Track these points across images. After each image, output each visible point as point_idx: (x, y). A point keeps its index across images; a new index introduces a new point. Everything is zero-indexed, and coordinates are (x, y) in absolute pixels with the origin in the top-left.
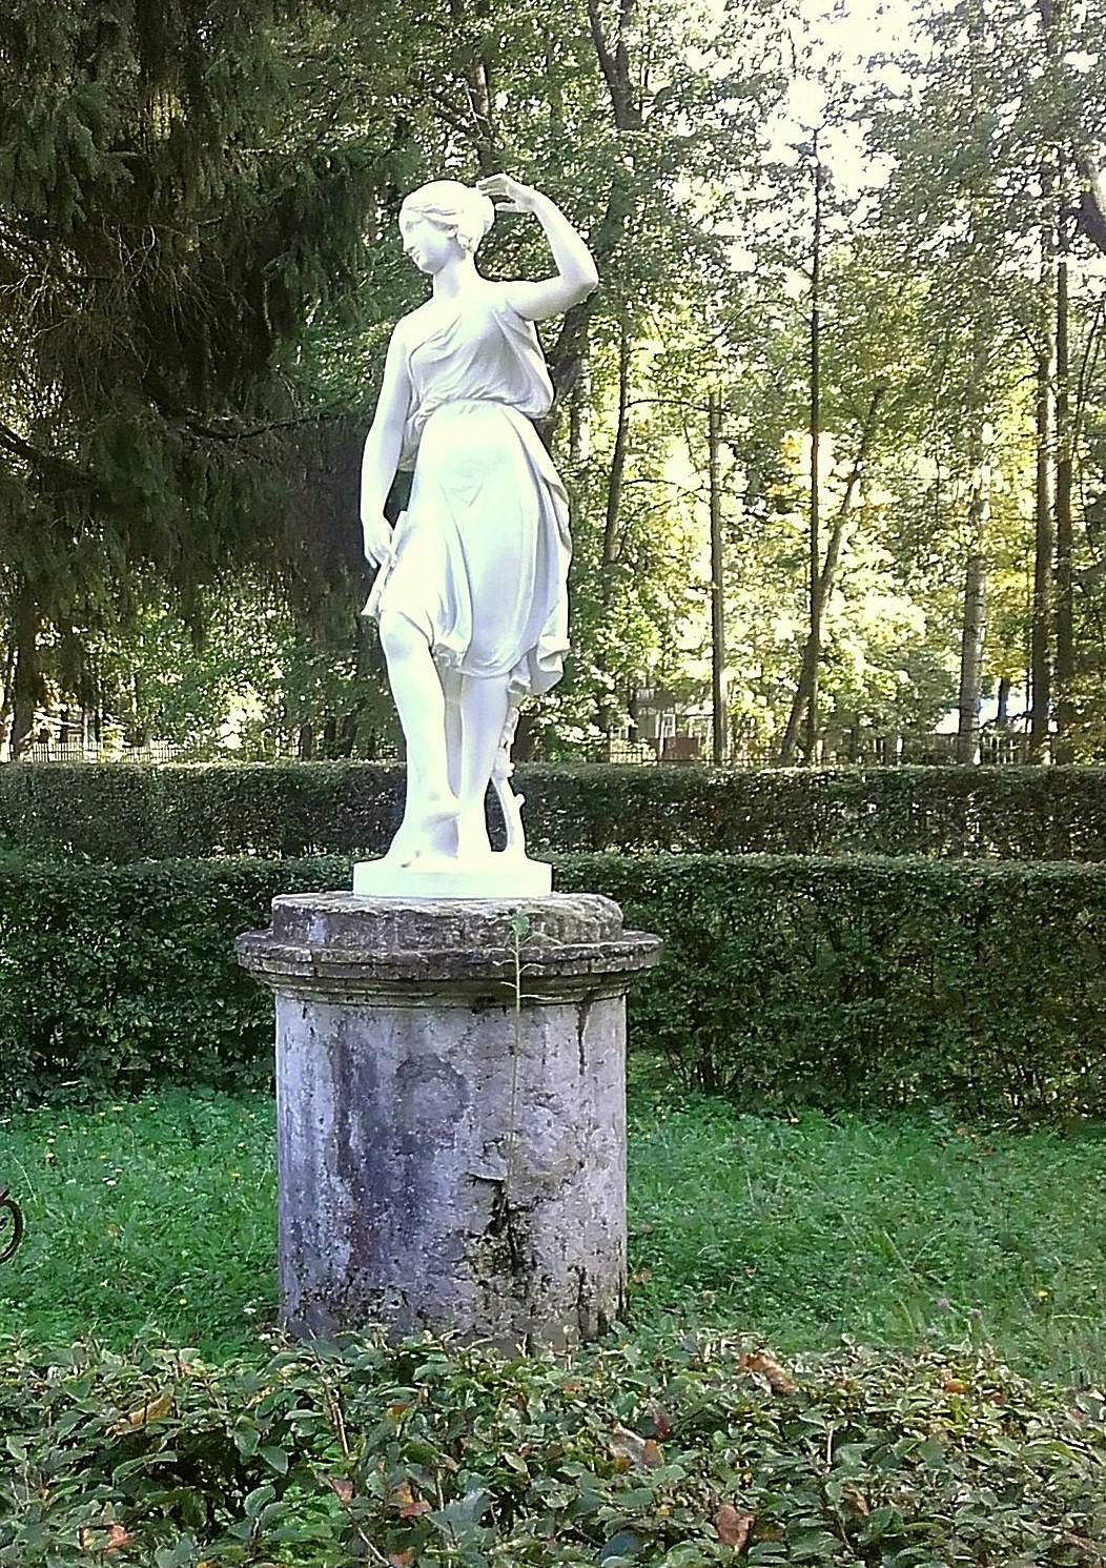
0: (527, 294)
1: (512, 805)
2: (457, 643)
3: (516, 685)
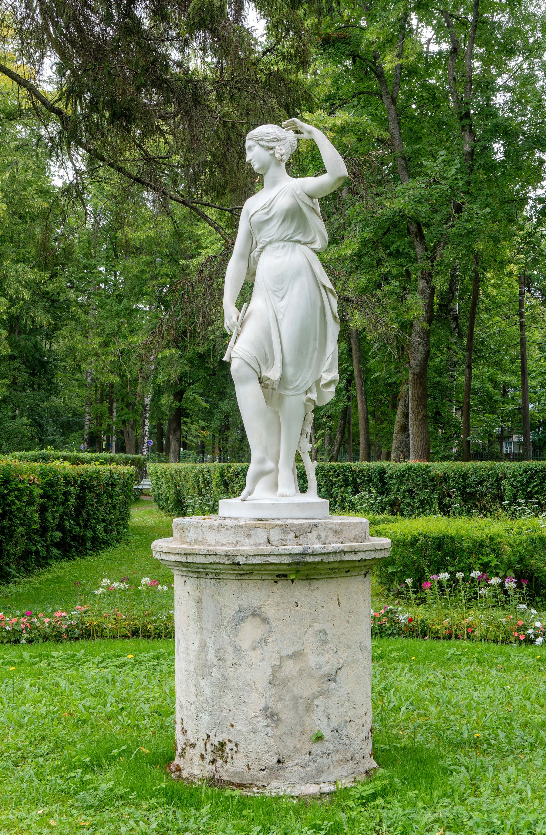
0: (310, 182)
1: (310, 467)
2: (273, 374)
3: (309, 400)
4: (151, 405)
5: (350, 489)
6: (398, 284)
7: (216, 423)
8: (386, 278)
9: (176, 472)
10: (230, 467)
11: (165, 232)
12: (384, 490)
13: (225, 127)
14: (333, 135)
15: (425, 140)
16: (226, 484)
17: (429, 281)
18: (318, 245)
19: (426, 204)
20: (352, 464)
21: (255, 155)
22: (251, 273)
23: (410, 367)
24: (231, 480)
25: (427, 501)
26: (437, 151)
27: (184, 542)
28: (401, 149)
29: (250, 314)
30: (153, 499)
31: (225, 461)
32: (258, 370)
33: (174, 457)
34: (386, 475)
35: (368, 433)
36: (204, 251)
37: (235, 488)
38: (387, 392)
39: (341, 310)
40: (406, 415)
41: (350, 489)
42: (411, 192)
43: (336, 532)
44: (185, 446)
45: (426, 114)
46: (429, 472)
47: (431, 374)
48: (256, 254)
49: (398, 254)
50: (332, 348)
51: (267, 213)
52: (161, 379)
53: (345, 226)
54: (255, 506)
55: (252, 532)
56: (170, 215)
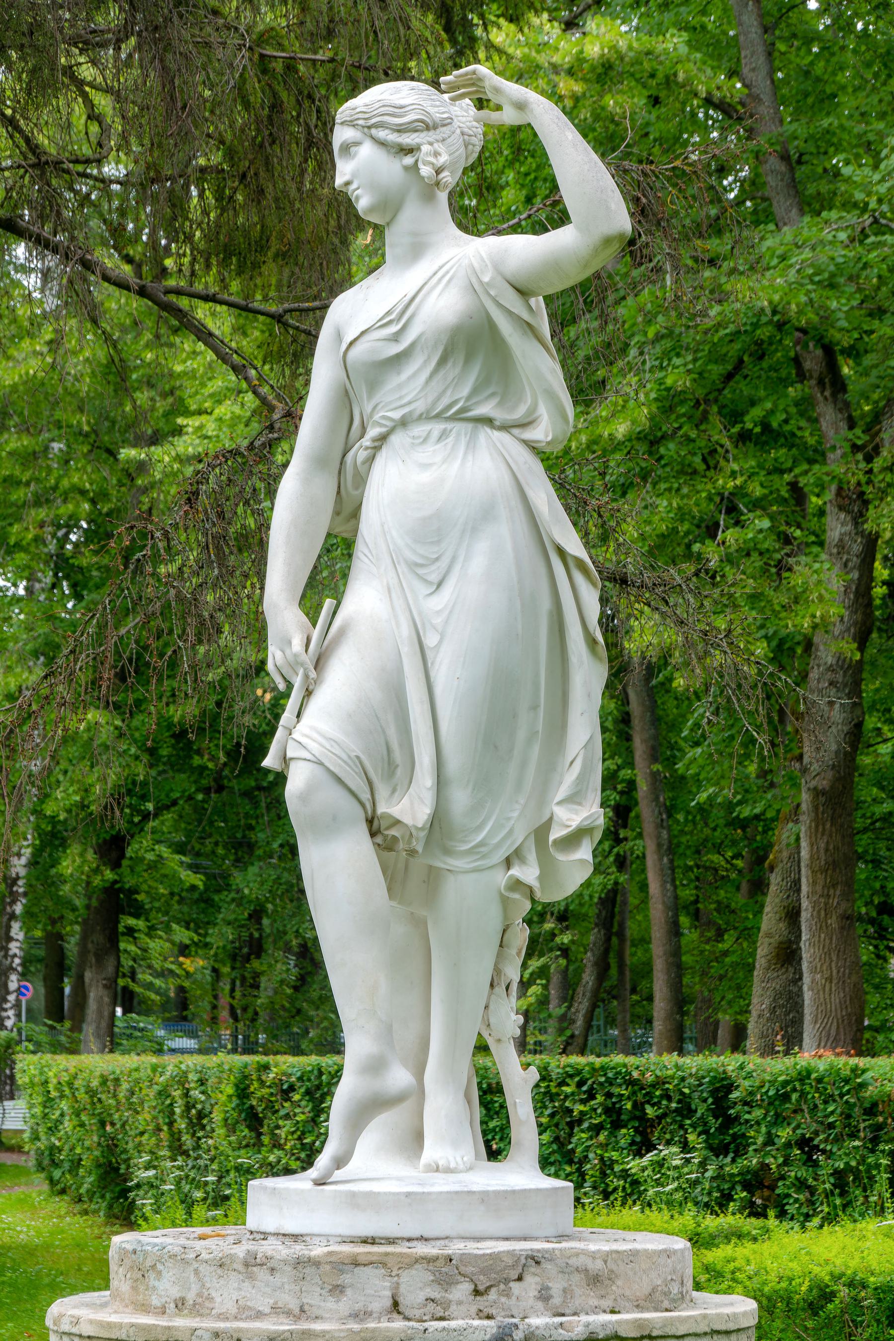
0: (522, 249)
1: (519, 1082)
2: (411, 808)
3: (517, 885)
4: (28, 877)
5: (625, 1135)
6: (766, 523)
7: (222, 935)
8: (731, 506)
9: (104, 1081)
10: (266, 1067)
11: (75, 366)
12: (726, 1140)
13: (265, 71)
14: (578, 88)
15: (848, 103)
16: (254, 1120)
17: (858, 518)
18: (541, 433)
19: (851, 288)
20: (632, 1060)
21: (359, 168)
22: (347, 510)
23: (804, 771)
24: (271, 1107)
25: (856, 1172)
26: (881, 136)
27: (144, 1308)
28: (776, 130)
29: (342, 632)
30: (32, 1162)
31: (250, 1049)
32: (365, 796)
33: (98, 1035)
34: (734, 1095)
35: (677, 968)
36: (190, 423)
37: (282, 1133)
38: (734, 843)
39: (607, 623)
40: (792, 915)
41: (625, 1135)
42: (807, 254)
43: (594, 1280)
44: (129, 1000)
45: (851, 25)
46: (863, 1086)
47: (866, 791)
48: (362, 455)
49: (767, 436)
50: (584, 731)
51: (396, 338)
52: (62, 800)
53: (612, 351)
54: (355, 1201)
55: (346, 1279)
56: (94, 316)
